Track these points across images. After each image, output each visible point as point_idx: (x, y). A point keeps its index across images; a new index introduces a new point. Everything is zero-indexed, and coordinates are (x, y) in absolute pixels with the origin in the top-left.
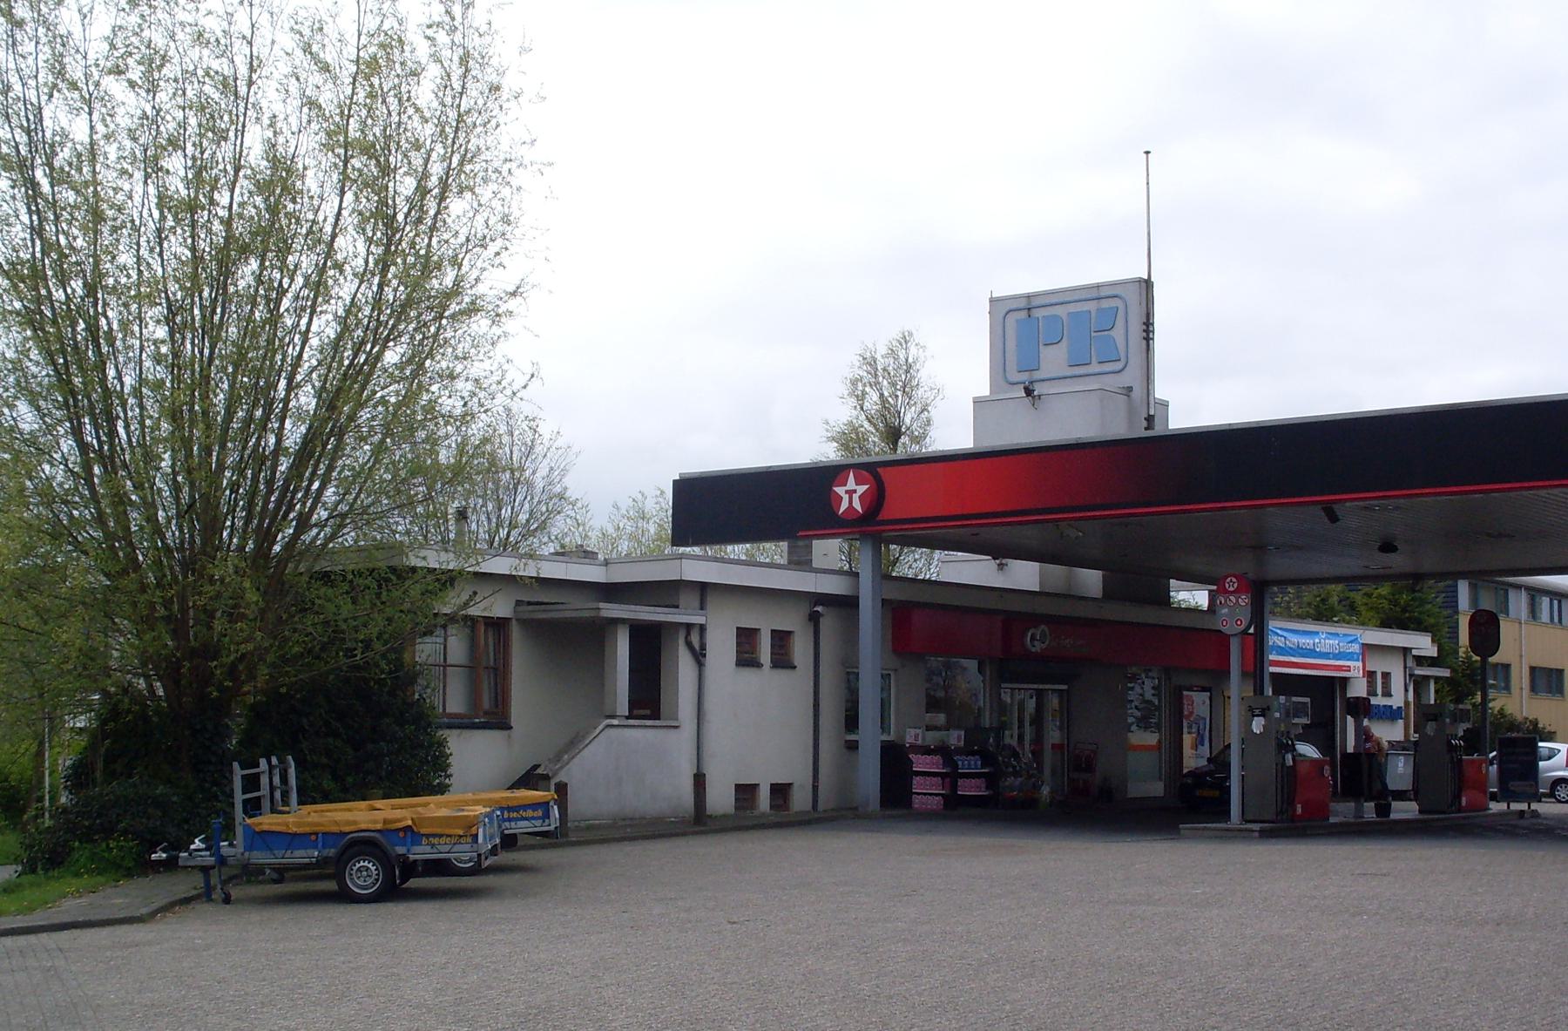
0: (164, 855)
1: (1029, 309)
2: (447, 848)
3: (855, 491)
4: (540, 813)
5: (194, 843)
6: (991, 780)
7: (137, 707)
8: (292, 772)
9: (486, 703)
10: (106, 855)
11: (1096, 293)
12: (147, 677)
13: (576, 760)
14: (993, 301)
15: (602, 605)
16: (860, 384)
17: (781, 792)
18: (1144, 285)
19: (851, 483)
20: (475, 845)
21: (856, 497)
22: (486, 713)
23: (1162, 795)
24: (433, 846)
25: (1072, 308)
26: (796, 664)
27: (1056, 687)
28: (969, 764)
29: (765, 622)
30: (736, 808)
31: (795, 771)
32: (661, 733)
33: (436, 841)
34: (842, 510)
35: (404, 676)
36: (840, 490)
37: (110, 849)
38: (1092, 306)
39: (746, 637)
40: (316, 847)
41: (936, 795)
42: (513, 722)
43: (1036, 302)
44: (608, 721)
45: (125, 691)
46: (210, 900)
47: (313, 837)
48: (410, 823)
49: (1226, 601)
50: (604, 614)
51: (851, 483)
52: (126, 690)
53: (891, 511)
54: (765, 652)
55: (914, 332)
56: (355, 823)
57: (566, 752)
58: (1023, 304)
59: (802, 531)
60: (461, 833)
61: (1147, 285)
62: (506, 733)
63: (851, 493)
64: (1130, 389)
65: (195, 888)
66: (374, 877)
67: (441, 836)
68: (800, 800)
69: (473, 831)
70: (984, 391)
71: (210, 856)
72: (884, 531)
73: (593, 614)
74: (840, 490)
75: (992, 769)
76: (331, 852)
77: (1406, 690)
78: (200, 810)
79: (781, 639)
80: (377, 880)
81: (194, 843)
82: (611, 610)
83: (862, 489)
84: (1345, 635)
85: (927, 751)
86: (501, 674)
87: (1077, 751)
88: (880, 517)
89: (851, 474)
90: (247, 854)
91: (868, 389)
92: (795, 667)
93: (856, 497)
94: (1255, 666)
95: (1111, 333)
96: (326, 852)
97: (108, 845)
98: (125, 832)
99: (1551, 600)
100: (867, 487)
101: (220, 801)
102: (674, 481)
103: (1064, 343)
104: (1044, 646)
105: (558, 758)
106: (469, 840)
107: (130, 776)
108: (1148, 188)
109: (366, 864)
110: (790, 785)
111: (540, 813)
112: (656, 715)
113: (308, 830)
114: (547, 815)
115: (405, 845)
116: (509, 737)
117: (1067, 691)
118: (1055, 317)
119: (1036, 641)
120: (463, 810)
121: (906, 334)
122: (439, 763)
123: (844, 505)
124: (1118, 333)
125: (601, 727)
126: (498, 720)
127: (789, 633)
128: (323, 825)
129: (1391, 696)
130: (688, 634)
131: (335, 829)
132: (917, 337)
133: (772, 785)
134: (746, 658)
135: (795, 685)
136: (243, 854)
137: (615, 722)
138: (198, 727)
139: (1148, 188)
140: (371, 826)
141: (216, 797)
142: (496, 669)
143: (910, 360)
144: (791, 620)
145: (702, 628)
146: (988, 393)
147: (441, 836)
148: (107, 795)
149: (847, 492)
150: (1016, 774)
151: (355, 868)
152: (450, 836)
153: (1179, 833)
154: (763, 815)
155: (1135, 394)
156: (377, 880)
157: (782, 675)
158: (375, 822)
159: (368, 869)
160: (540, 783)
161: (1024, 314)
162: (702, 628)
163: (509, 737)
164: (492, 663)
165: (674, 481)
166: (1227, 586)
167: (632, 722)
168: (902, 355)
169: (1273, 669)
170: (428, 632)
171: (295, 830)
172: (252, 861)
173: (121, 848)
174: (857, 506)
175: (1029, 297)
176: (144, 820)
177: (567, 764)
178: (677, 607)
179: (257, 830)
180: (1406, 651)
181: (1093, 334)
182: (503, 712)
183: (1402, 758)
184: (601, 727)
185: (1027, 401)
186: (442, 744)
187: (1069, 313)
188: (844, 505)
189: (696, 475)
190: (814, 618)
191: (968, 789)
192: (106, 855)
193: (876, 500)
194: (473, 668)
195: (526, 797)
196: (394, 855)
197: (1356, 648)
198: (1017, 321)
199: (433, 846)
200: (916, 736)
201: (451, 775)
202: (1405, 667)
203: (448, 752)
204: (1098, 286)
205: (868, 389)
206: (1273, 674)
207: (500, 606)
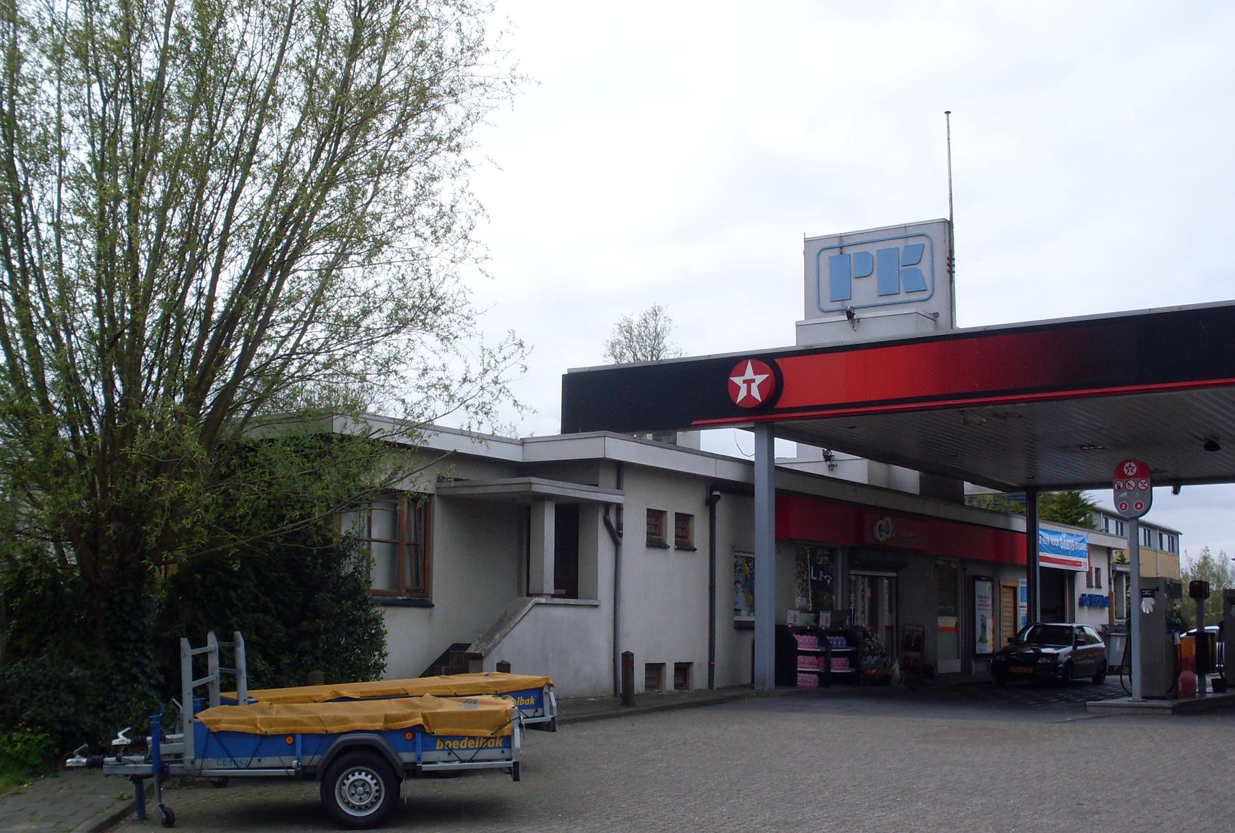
0: (84, 760)
1: (841, 247)
2: (469, 754)
3: (753, 381)
4: (532, 701)
5: (117, 737)
6: (853, 659)
7: (49, 575)
8: (241, 651)
9: (408, 581)
10: (8, 749)
11: (904, 233)
12: (57, 540)
13: (506, 639)
14: (807, 242)
15: (533, 480)
16: (618, 347)
17: (683, 670)
18: (947, 225)
19: (749, 373)
20: (506, 750)
21: (754, 387)
22: (407, 591)
23: (959, 670)
24: (451, 751)
25: (882, 246)
26: (695, 546)
27: (868, 573)
28: (842, 645)
29: (673, 503)
30: (647, 687)
31: (696, 654)
32: (582, 612)
33: (454, 744)
34: (739, 399)
35: (332, 554)
36: (738, 380)
37: (11, 743)
38: (900, 244)
39: (655, 517)
40: (293, 754)
41: (813, 673)
42: (435, 600)
43: (846, 242)
44: (536, 600)
45: (35, 558)
46: (143, 818)
47: (289, 740)
48: (420, 721)
49: (1124, 485)
50: (536, 488)
51: (749, 373)
52: (36, 556)
53: (786, 401)
54: (670, 538)
55: (664, 307)
56: (344, 720)
57: (497, 631)
58: (836, 243)
59: (696, 420)
60: (488, 733)
61: (949, 225)
62: (428, 611)
63: (749, 382)
64: (936, 315)
65: (121, 798)
66: (373, 793)
67: (460, 738)
68: (699, 679)
69: (506, 731)
70: (802, 318)
71: (146, 762)
72: (779, 419)
73: (524, 488)
74: (738, 380)
75: (854, 648)
76: (315, 760)
77: (1110, 583)
78: (118, 694)
79: (683, 520)
80: (377, 798)
81: (117, 737)
82: (542, 485)
83: (760, 378)
84: (1077, 536)
85: (802, 631)
86: (422, 551)
87: (906, 633)
88: (778, 406)
89: (749, 363)
90: (198, 762)
91: (625, 351)
92: (696, 550)
93: (754, 387)
94: (1028, 562)
95: (918, 266)
96: (307, 760)
97: (10, 738)
98: (32, 722)
99: (1117, 522)
100: (767, 376)
101: (141, 683)
102: (563, 376)
103: (874, 277)
104: (888, 536)
105: (489, 636)
106: (499, 743)
107: (37, 654)
108: (949, 143)
109: (363, 776)
110: (690, 664)
111: (532, 701)
112: (575, 596)
113: (281, 730)
114: (539, 703)
115: (414, 750)
116: (430, 614)
117: (896, 578)
118: (866, 253)
119: (883, 532)
120: (475, 702)
121: (657, 309)
122: (375, 641)
123: (742, 394)
124: (924, 267)
125: (530, 605)
126: (419, 598)
127: (690, 516)
128: (302, 724)
129: (1101, 587)
130: (607, 513)
131: (318, 729)
132: (665, 312)
133: (676, 664)
134: (655, 541)
135: (696, 563)
136: (193, 763)
137: (543, 600)
138: (117, 599)
139: (949, 143)
140: (368, 726)
141: (135, 679)
142: (416, 546)
143: (659, 329)
144: (691, 504)
145: (619, 507)
146: (803, 319)
147: (460, 738)
148: (10, 676)
149: (745, 382)
150: (872, 653)
151: (348, 783)
152: (474, 738)
153: (1085, 711)
154: (670, 695)
155: (940, 319)
156: (377, 798)
157: (685, 556)
158: (373, 719)
159: (365, 783)
160: (472, 663)
161: (836, 252)
162: (619, 507)
163: (430, 614)
164: (413, 540)
165: (563, 376)
166: (1126, 471)
167: (557, 600)
168: (652, 323)
169: (1042, 564)
170: (353, 506)
171: (264, 730)
172: (207, 772)
173: (26, 742)
174: (756, 393)
175: (841, 237)
176: (54, 708)
177: (499, 642)
178: (597, 486)
179: (213, 729)
180: (1109, 550)
181: (901, 268)
182: (424, 591)
183: (1119, 638)
184: (530, 605)
185: (848, 324)
186: (377, 620)
187: (878, 251)
188: (742, 394)
189: (587, 370)
190: (710, 503)
191: (839, 667)
192: (8, 749)
193: (774, 389)
194: (394, 544)
195: (516, 683)
196: (401, 764)
197: (1084, 547)
198: (830, 257)
199: (451, 751)
200: (795, 618)
201: (386, 655)
202: (1109, 565)
203: (384, 629)
204: (906, 227)
205: (625, 351)
206: (1042, 568)
207: (422, 482)
